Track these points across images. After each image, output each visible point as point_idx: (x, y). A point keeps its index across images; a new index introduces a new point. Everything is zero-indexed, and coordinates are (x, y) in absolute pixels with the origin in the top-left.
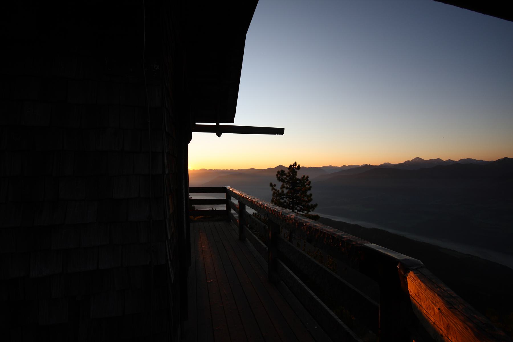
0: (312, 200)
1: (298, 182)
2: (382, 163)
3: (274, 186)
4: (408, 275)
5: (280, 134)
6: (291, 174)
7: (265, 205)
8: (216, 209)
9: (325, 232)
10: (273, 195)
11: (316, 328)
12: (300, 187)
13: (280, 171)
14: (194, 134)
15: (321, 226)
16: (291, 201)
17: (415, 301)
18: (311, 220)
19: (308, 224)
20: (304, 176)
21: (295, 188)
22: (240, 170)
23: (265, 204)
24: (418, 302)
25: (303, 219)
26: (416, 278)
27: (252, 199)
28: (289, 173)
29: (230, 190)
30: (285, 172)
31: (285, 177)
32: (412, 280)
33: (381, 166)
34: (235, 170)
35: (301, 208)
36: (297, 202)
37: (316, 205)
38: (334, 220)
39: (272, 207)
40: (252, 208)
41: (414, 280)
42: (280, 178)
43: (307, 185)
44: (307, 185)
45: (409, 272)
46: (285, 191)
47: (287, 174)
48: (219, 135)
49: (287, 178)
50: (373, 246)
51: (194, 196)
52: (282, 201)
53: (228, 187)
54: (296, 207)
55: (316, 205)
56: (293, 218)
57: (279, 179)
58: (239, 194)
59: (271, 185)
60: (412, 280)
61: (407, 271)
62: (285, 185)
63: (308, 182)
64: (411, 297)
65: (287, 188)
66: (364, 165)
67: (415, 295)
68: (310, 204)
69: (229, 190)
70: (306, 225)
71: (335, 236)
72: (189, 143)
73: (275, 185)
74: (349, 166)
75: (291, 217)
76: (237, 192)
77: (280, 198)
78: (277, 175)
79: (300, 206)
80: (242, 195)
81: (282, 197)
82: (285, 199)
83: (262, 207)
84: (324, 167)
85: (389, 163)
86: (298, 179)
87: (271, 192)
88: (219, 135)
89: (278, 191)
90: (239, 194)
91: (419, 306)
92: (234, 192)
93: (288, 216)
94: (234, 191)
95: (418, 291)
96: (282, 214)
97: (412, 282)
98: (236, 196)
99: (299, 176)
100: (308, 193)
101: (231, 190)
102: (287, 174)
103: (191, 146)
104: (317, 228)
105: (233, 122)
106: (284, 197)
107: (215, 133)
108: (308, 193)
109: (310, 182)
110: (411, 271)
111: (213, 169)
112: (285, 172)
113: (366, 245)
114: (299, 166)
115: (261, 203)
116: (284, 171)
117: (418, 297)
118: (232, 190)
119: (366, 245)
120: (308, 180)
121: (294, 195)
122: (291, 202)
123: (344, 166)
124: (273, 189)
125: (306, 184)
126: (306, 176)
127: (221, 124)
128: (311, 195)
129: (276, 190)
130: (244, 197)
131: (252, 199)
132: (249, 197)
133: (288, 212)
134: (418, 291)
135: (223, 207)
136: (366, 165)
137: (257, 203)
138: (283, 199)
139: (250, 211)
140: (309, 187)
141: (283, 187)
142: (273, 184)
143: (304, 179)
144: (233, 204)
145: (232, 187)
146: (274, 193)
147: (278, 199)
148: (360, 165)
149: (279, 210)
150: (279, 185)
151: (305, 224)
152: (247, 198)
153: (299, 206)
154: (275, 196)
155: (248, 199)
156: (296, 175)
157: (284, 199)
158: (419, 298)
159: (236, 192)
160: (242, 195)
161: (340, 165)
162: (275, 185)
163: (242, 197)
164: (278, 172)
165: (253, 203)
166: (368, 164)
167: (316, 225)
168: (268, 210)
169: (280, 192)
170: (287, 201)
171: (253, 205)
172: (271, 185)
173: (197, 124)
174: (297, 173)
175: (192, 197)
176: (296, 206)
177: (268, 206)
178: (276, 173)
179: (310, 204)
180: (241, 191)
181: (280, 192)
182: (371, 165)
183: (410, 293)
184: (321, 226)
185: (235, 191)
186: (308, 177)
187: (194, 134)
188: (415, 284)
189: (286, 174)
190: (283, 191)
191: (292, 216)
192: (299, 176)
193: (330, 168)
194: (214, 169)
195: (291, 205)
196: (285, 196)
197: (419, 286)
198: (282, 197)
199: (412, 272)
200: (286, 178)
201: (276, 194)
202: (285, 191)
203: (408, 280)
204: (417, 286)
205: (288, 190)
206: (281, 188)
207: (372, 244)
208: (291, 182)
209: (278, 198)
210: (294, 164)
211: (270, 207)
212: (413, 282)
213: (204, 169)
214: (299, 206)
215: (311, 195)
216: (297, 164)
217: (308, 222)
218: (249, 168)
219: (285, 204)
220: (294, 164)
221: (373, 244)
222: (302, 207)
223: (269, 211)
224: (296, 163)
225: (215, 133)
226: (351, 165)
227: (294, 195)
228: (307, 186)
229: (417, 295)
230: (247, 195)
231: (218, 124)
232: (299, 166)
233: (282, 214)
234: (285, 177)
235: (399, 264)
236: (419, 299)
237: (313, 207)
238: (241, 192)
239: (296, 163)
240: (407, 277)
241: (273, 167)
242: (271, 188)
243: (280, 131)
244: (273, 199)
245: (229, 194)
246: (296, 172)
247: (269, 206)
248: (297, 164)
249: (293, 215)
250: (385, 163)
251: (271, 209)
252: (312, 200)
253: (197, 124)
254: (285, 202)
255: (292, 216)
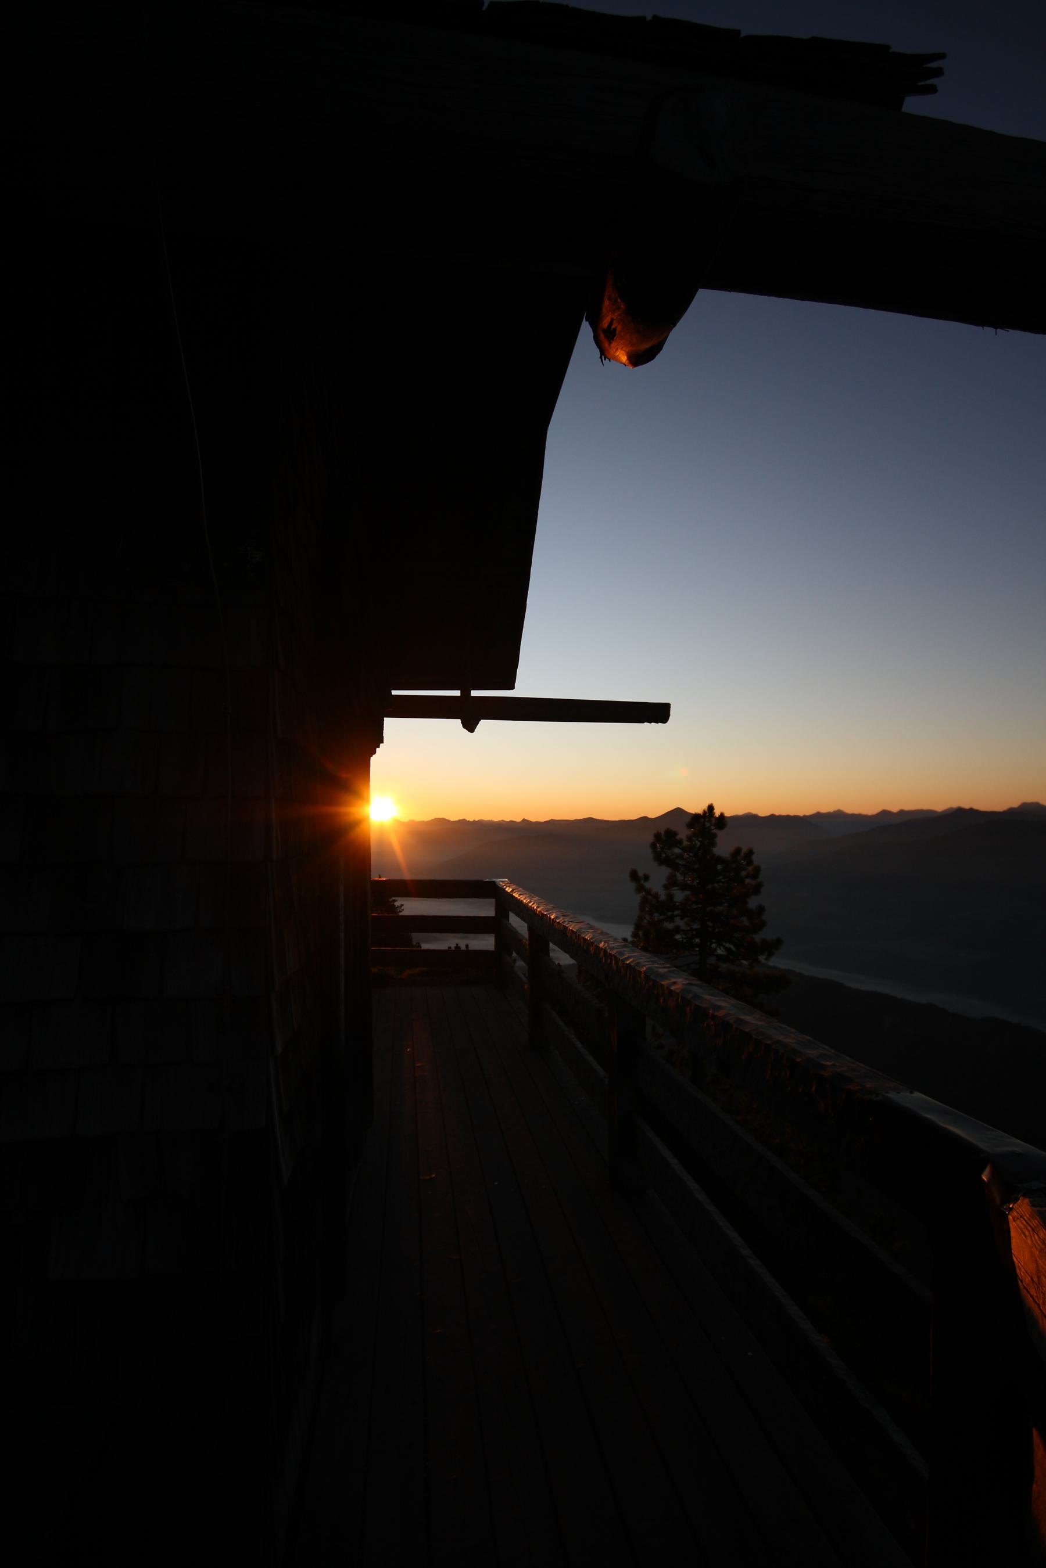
0: (763, 924)
1: (719, 867)
2: (1015, 804)
3: (642, 882)
4: (1011, 1209)
5: (657, 722)
6: (699, 844)
7: (602, 945)
8: (467, 946)
9: (769, 1042)
10: (642, 908)
11: (750, 1354)
12: (726, 885)
13: (663, 833)
14: (392, 726)
15: (759, 1023)
16: (696, 926)
17: (1031, 1299)
18: (733, 1001)
19: (720, 1014)
20: (738, 851)
21: (710, 887)
22: (746, 814)
23: (601, 942)
24: (1038, 1305)
25: (708, 997)
26: (1035, 1222)
27: (565, 922)
28: (689, 839)
29: (507, 889)
30: (678, 837)
31: (677, 851)
32: (1022, 1226)
33: (1011, 812)
34: (537, 823)
35: (728, 950)
36: (717, 930)
37: (778, 943)
38: (853, 985)
39: (621, 952)
40: (566, 952)
41: (1029, 1228)
42: (664, 855)
43: (747, 876)
44: (747, 876)
45: (1018, 1199)
46: (679, 896)
47: (686, 843)
48: (470, 726)
49: (686, 855)
50: (914, 1100)
51: (411, 907)
52: (669, 926)
53: (502, 882)
54: (714, 946)
55: (778, 943)
56: (678, 991)
57: (661, 859)
58: (530, 905)
59: (634, 876)
60: (1022, 1226)
61: (1011, 1195)
62: (680, 877)
63: (750, 868)
64: (1020, 1282)
65: (684, 887)
66: (951, 808)
67: (1030, 1279)
68: (758, 938)
69: (504, 890)
70: (714, 1017)
71: (799, 1060)
72: (375, 753)
73: (646, 878)
74: (902, 812)
75: (673, 988)
76: (525, 899)
77: (662, 917)
78: (653, 846)
79: (728, 945)
80: (539, 910)
81: (670, 914)
82: (678, 921)
83: (592, 949)
84: (818, 816)
85: (750, 813)
86: (720, 860)
87: (638, 898)
88: (470, 726)
89: (656, 896)
90: (530, 905)
91: (1040, 1321)
92: (517, 896)
93: (662, 983)
94: (516, 895)
95: (1037, 1266)
96: (647, 977)
97: (1023, 1236)
98: (523, 910)
99: (723, 847)
100: (753, 903)
101: (509, 890)
102: (686, 843)
103: (480, 722)
104: (747, 1030)
105: (511, 687)
106: (677, 916)
107: (459, 721)
108: (753, 903)
109: (757, 869)
110: (1024, 1196)
111: (470, 818)
112: (678, 837)
113: (889, 1095)
114: (722, 815)
115: (588, 937)
116: (675, 834)
117: (1038, 1287)
118: (512, 891)
119: (892, 1095)
120: (750, 863)
121: (708, 909)
122: (696, 929)
123: (885, 813)
124: (640, 889)
125: (743, 874)
126: (744, 850)
127: (475, 693)
128: (761, 909)
129: (648, 892)
130: (543, 914)
131: (565, 922)
132: (556, 918)
133: (666, 970)
134: (1037, 1266)
135: (486, 943)
136: (960, 810)
137: (579, 935)
138: (671, 919)
139: (561, 957)
140: (753, 882)
141: (671, 882)
142: (640, 874)
143: (739, 858)
144: (514, 932)
145: (512, 882)
146: (644, 902)
147: (656, 919)
148: (496, 820)
149: (639, 963)
150: (658, 877)
151: (713, 1014)
152: (552, 917)
153: (724, 944)
154: (647, 909)
155: (554, 921)
156: (714, 844)
157: (674, 922)
158: (1042, 1292)
159: (521, 898)
160: (538, 907)
161: (870, 808)
162: (646, 878)
163: (538, 915)
164: (657, 836)
165: (567, 936)
166: (967, 806)
167: (743, 1017)
168: (609, 961)
169: (663, 897)
170: (683, 927)
171: (570, 942)
172: (634, 876)
173: (394, 692)
174: (717, 840)
175: (402, 905)
176: (711, 943)
177: (609, 948)
178: (651, 839)
179: (758, 938)
180: (537, 896)
181: (663, 897)
182: (780, 816)
183: (1018, 1271)
184: (759, 1023)
185: (520, 894)
186: (750, 852)
187: (392, 726)
188: (1029, 1241)
189: (680, 842)
190: (670, 897)
191: (675, 983)
192: (723, 847)
193: (838, 818)
194: (472, 820)
195: (697, 940)
196: (676, 913)
197: (1040, 1252)
198: (670, 914)
199: (1027, 1201)
200: (681, 856)
201: (650, 904)
202: (679, 896)
203: (1011, 1225)
204: (1034, 1250)
205: (688, 893)
206: (666, 887)
207: (912, 1093)
208: (697, 866)
209: (656, 916)
210: (706, 809)
211: (613, 952)
212: (1026, 1237)
213: (443, 821)
214: (724, 944)
215: (761, 909)
216: (717, 813)
217: (720, 1008)
218: (578, 818)
219: (678, 937)
220: (705, 812)
221: (917, 1095)
222: (732, 947)
223: (611, 963)
224: (711, 808)
225: (459, 721)
226: (907, 808)
227: (708, 909)
228: (748, 881)
229: (1035, 1279)
230: (554, 908)
231: (466, 693)
232: (722, 815)
233: (647, 977)
234: (677, 851)
235: (987, 1170)
236: (1042, 1294)
237: (772, 947)
238: (535, 898)
239: (711, 808)
240: (1010, 1217)
241: (653, 814)
242: (632, 886)
243: (658, 713)
244: (641, 918)
245: (505, 904)
246: (715, 836)
247: (612, 949)
248: (717, 813)
249: (680, 980)
250: (1024, 806)
251: (616, 957)
252: (763, 924)
253: (394, 692)
254: (678, 930)
255: (675, 983)
